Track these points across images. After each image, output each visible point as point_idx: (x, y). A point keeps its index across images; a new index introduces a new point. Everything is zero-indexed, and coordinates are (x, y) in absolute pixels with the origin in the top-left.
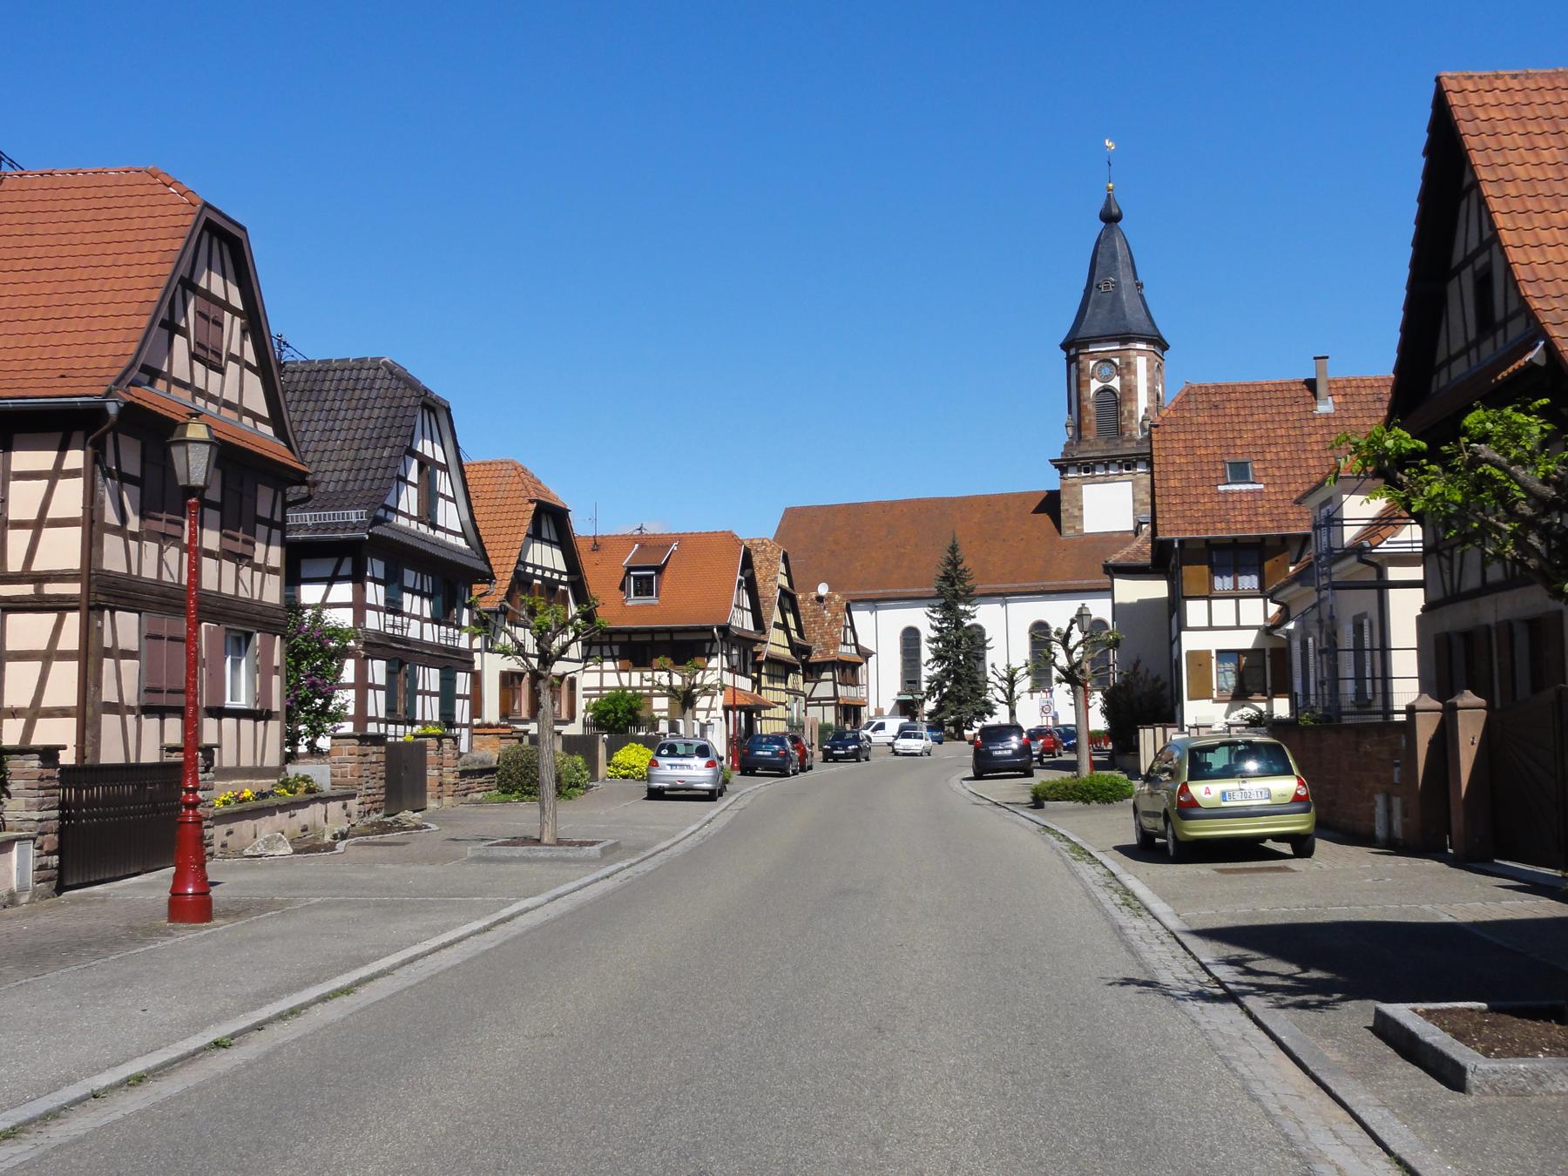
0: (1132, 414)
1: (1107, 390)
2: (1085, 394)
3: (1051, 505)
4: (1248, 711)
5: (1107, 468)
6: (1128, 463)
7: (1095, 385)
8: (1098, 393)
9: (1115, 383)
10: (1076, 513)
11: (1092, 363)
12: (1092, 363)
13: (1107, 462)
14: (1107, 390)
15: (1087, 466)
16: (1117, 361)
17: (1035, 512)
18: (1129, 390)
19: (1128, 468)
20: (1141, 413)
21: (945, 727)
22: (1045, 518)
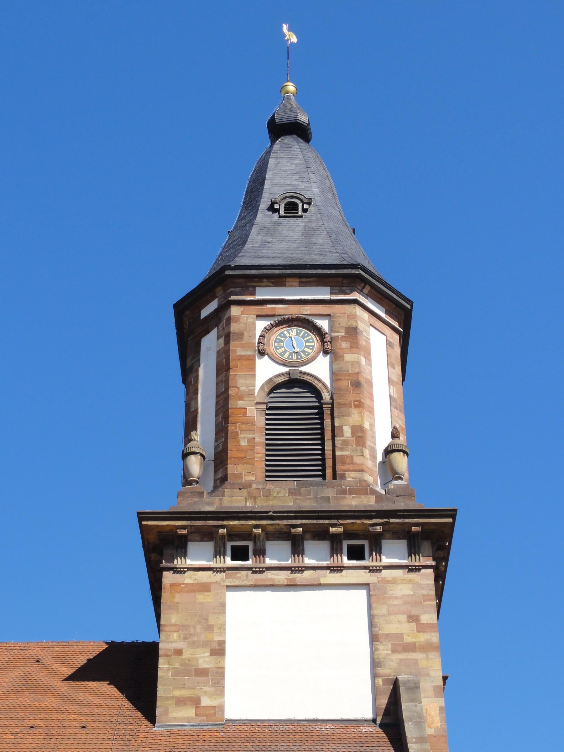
0: (360, 436)
1: (295, 382)
2: (239, 381)
3: (131, 670)
4: (312, 161)
5: (297, 549)
6: (354, 537)
7: (266, 370)
8: (275, 387)
9: (320, 369)
10: (204, 660)
11: (261, 325)
12: (261, 325)
13: (301, 531)
14: (295, 382)
15: (242, 540)
16: (324, 324)
17: (85, 673)
18: (355, 384)
19: (356, 553)
20: (382, 439)
21: (255, 497)
22: (105, 696)
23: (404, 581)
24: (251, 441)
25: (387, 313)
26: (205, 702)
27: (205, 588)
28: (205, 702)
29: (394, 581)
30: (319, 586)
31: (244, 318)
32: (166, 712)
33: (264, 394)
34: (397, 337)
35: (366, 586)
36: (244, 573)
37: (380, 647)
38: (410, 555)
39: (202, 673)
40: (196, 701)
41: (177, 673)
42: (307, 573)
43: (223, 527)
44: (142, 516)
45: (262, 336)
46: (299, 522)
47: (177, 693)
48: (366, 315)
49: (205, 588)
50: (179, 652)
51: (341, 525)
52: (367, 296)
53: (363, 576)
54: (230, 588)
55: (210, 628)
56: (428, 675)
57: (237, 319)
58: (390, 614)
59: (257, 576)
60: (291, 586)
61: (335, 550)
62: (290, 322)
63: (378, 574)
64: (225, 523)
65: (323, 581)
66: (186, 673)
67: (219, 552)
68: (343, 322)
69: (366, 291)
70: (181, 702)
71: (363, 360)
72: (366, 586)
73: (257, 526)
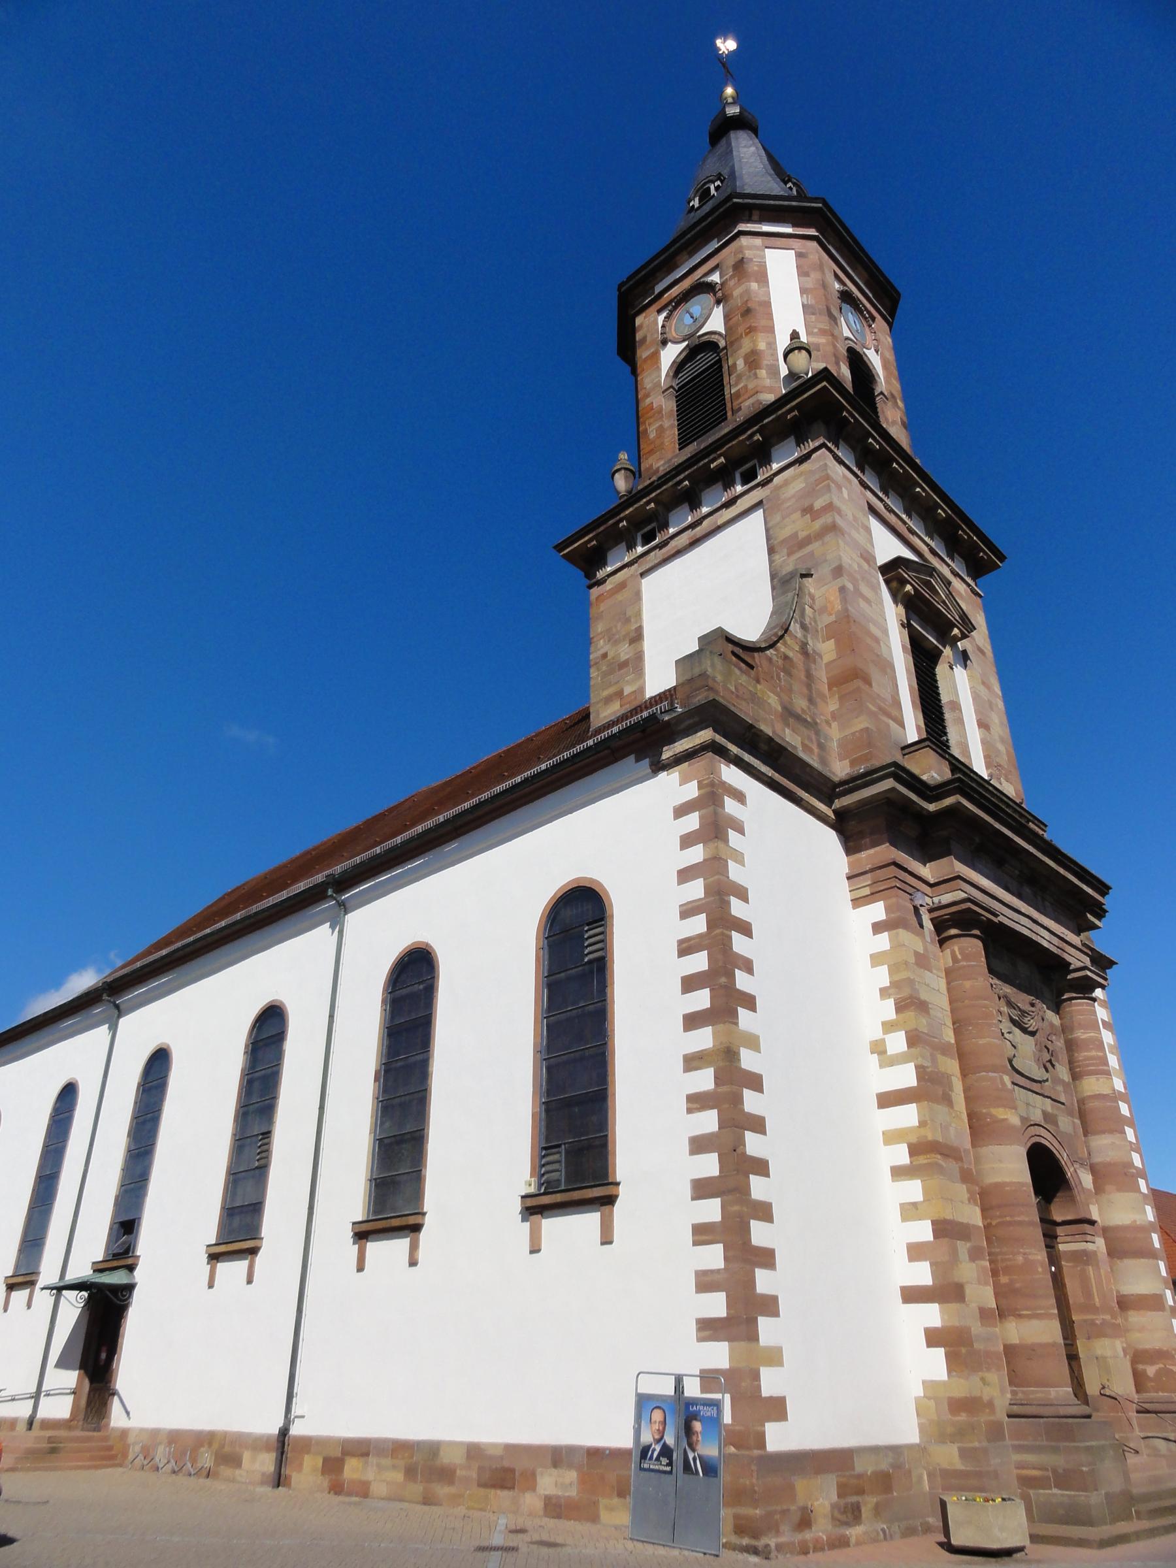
10: (624, 651)
12: (661, 318)
23: (794, 478)
24: (661, 430)
25: (794, 225)
26: (628, 690)
27: (622, 586)
28: (628, 690)
29: (786, 483)
30: (718, 529)
31: (647, 322)
32: (598, 713)
33: (669, 379)
34: (814, 245)
35: (759, 504)
36: (652, 554)
37: (777, 557)
38: (798, 445)
39: (624, 664)
40: (619, 694)
41: (605, 675)
42: (705, 523)
43: (621, 520)
44: (559, 547)
45: (663, 326)
46: (682, 476)
47: (605, 693)
48: (758, 241)
49: (622, 586)
50: (605, 656)
51: (719, 457)
52: (761, 221)
53: (757, 495)
54: (643, 575)
55: (628, 620)
56: (826, 561)
57: (641, 326)
58: (783, 519)
59: (664, 550)
60: (695, 543)
61: (728, 484)
62: (686, 297)
63: (770, 485)
64: (622, 515)
65: (720, 522)
66: (611, 672)
67: (631, 547)
68: (731, 261)
69: (755, 217)
70: (608, 700)
71: (754, 286)
72: (759, 504)
73: (648, 503)
